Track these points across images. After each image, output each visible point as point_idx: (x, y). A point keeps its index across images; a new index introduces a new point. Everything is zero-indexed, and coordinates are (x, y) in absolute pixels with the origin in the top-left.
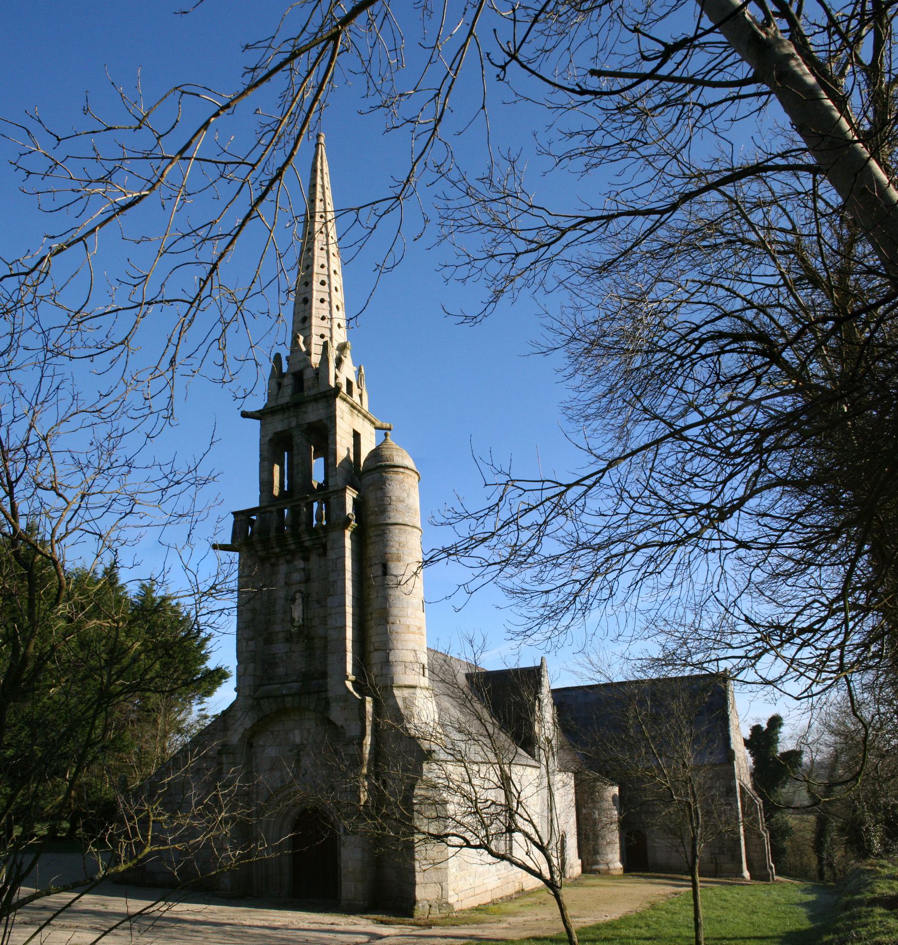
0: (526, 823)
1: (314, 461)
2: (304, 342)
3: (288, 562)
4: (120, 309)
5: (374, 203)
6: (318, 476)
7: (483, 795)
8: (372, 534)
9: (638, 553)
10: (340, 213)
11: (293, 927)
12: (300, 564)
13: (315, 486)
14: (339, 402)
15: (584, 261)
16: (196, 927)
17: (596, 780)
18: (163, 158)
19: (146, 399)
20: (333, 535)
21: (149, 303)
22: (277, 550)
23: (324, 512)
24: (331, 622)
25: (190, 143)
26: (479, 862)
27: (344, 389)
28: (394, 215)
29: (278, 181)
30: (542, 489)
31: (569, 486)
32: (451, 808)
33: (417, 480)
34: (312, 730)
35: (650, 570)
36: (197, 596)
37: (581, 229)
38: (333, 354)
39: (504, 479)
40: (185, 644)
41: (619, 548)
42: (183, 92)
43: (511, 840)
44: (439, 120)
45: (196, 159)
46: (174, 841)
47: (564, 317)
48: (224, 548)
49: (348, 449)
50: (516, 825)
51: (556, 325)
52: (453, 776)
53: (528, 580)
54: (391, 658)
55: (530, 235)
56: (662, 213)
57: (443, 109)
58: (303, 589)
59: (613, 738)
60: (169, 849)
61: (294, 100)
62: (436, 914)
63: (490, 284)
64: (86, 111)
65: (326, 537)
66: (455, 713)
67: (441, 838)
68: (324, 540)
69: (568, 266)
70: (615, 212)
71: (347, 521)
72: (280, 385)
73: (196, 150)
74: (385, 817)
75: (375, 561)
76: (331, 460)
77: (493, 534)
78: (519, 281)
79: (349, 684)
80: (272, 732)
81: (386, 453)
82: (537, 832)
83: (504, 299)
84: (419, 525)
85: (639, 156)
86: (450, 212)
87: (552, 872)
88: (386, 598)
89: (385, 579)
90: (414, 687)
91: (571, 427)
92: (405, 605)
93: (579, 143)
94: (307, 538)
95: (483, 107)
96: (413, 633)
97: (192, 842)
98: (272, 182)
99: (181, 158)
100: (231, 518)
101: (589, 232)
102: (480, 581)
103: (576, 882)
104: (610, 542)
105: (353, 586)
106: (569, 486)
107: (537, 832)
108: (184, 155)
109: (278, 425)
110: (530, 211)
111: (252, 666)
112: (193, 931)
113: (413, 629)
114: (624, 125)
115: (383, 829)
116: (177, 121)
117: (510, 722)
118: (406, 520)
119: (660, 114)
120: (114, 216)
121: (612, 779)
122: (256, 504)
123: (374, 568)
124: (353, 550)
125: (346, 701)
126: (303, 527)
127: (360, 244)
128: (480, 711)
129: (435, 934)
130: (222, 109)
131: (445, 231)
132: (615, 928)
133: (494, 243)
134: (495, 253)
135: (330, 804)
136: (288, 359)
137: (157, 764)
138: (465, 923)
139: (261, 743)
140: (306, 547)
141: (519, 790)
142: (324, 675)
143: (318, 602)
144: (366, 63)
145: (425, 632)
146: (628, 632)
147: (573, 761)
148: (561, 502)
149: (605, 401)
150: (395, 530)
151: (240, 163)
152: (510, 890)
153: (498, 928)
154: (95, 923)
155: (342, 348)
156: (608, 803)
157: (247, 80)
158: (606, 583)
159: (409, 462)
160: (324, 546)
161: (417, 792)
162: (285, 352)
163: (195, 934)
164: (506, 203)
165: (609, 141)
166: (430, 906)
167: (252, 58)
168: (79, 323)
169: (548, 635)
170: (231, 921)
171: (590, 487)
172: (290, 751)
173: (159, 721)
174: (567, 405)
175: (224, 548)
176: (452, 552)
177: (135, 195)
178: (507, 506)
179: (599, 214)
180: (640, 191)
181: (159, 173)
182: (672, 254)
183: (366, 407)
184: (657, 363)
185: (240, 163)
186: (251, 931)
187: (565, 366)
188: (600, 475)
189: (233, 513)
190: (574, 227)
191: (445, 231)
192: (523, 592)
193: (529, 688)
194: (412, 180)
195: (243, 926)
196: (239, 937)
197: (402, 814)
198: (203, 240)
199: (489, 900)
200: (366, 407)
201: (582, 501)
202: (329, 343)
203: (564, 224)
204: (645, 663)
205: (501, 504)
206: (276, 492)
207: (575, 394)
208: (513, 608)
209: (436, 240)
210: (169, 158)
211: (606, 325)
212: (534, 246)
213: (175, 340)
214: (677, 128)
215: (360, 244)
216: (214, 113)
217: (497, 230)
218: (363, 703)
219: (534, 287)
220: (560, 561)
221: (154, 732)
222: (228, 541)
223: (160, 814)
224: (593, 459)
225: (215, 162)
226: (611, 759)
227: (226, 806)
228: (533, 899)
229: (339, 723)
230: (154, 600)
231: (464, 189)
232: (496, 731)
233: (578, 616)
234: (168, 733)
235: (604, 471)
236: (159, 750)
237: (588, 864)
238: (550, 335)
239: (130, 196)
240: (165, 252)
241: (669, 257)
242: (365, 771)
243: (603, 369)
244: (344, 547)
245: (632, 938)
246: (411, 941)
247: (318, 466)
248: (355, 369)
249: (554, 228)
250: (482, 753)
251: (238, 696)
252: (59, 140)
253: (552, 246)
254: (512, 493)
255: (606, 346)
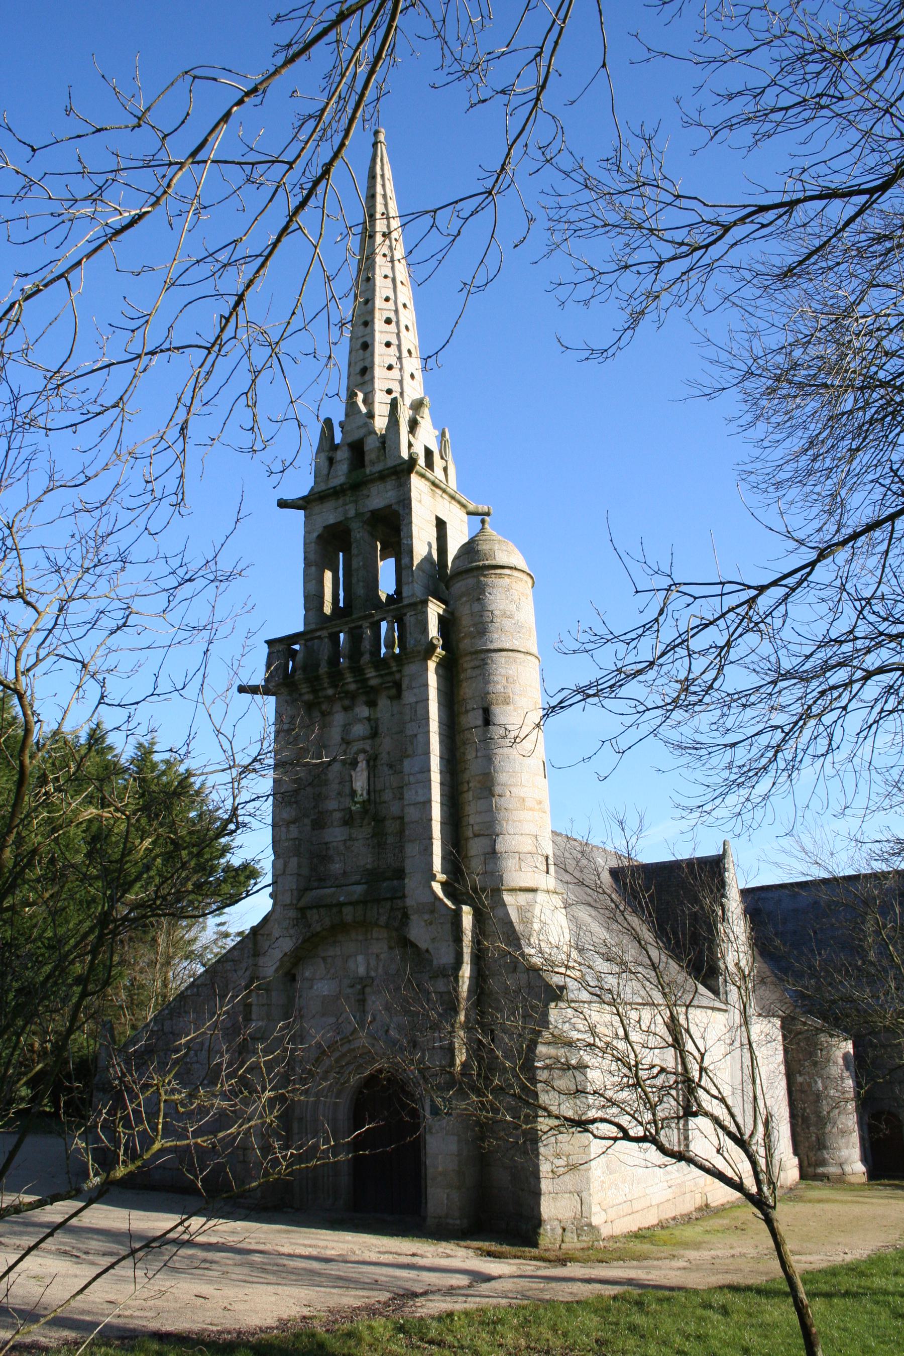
0: (715, 1102)
1: (381, 564)
2: (365, 401)
3: (346, 709)
4: (113, 364)
5: (456, 202)
6: (386, 585)
7: (647, 1058)
8: (465, 665)
9: (869, 682)
10: (408, 218)
11: (353, 1258)
12: (363, 711)
13: (383, 598)
14: (414, 478)
15: (759, 267)
16: (210, 1255)
17: (819, 1031)
18: (170, 164)
19: (147, 482)
20: (410, 669)
21: (153, 353)
22: (330, 692)
23: (396, 634)
24: (410, 795)
25: (205, 141)
26: (643, 1163)
27: (421, 461)
28: (486, 215)
29: (324, 182)
30: (722, 595)
31: (762, 589)
32: (593, 1075)
33: (530, 585)
34: (382, 956)
35: (889, 707)
36: (235, 772)
37: (752, 222)
38: (405, 415)
39: (666, 582)
40: (223, 840)
41: (840, 676)
42: (195, 77)
43: (686, 1130)
44: (543, 87)
45: (213, 162)
46: (196, 1134)
47: (735, 345)
48: (253, 690)
49: (430, 544)
50: (699, 1105)
51: (724, 357)
52: (600, 1029)
53: (704, 728)
54: (499, 847)
55: (679, 236)
56: (871, 191)
57: (548, 72)
58: (368, 748)
59: (844, 965)
60: (189, 1145)
61: (343, 75)
62: (572, 1243)
63: (624, 304)
64: (68, 111)
65: (400, 671)
66: (599, 932)
67: (582, 1124)
68: (397, 676)
69: (737, 275)
70: (801, 195)
71: (432, 647)
72: (331, 461)
73: (213, 151)
74: (499, 1091)
75: (471, 705)
76: (405, 561)
77: (652, 663)
78: (666, 299)
79: (437, 887)
80: (324, 959)
81: (484, 547)
82: (732, 1116)
83: (646, 323)
84: (534, 650)
85: (833, 114)
86: (563, 212)
87: (758, 1182)
88: (489, 759)
89: (487, 731)
90: (533, 890)
91: (755, 499)
92: (518, 769)
93: (740, 106)
94: (374, 674)
95: (604, 65)
96: (531, 809)
97: (221, 1135)
98: (316, 183)
99: (193, 163)
100: (265, 649)
101: (763, 226)
102: (633, 735)
103: (792, 1194)
104: (826, 668)
105: (441, 742)
106: (762, 589)
107: (732, 1116)
108: (198, 158)
109: (329, 515)
110: (677, 203)
111: (294, 862)
112: (205, 1261)
113: (529, 803)
114: (808, 77)
115: (496, 1111)
116: (188, 114)
117: (684, 945)
118: (516, 644)
119: (860, 56)
120: (106, 242)
121: (845, 1030)
122: (300, 628)
123: (471, 715)
124: (439, 690)
125: (432, 912)
126: (366, 658)
127: (439, 256)
128: (638, 929)
129: (572, 1275)
130: (248, 94)
131: (557, 238)
132: (862, 1274)
133: (628, 250)
134: (629, 263)
135: (413, 1071)
136: (341, 424)
137: (156, 1004)
138: (620, 1259)
139: (307, 974)
140: (372, 687)
141: (703, 1051)
142: (400, 874)
143: (391, 766)
144: (439, 25)
145: (547, 805)
146: (860, 801)
147: (781, 1001)
148: (751, 613)
149: (804, 461)
150: (500, 658)
151: (273, 162)
152: (688, 1205)
153: (671, 1269)
154: (64, 1244)
155: (417, 406)
156: (837, 1068)
157: (280, 59)
158: (821, 728)
159: (515, 558)
160: (398, 685)
161: (542, 1049)
162: (338, 414)
163: (207, 1265)
164: (642, 195)
165: (787, 100)
166: (564, 1230)
167: (286, 32)
168: (58, 386)
169: (737, 810)
170: (261, 1247)
171: (793, 590)
172: (352, 986)
173: (160, 940)
174: (748, 468)
175: (253, 690)
176: (591, 692)
177: (133, 213)
178: (671, 622)
179: (777, 199)
180: (835, 164)
181: (164, 183)
182: (890, 250)
183: (453, 484)
184: (877, 404)
185: (273, 162)
186: (292, 1263)
187: (741, 413)
188: (808, 570)
189: (266, 642)
190: (742, 220)
191: (557, 238)
192: (697, 746)
193: (712, 891)
194: (508, 168)
195: (281, 1254)
196: (274, 1273)
197: (524, 1088)
198: (225, 266)
199: (655, 1222)
200: (453, 484)
201: (782, 608)
202: (400, 400)
203: (727, 217)
204: (887, 847)
205: (661, 619)
206: (328, 609)
207: (757, 452)
208: (683, 771)
209: (546, 250)
210: (177, 163)
211: (797, 353)
212: (684, 249)
213: (186, 400)
214: (887, 75)
215: (439, 256)
216: (236, 100)
217: (631, 232)
218: (457, 916)
219: (688, 305)
220: (753, 699)
221: (153, 957)
222: (259, 679)
223: (173, 1091)
224: (793, 545)
225: (240, 163)
226: (841, 999)
227: (270, 1082)
228: (725, 1222)
229: (423, 945)
230: (154, 766)
231: (582, 181)
232: (664, 958)
233: (781, 780)
234: (172, 958)
235: (813, 564)
236: (159, 983)
237: (809, 1165)
238: (715, 370)
239: (127, 214)
240: (173, 284)
241: (886, 254)
242: (462, 1017)
243: (797, 413)
244: (426, 685)
245: (893, 1294)
246: (534, 1286)
247: (386, 570)
248: (437, 433)
249: (713, 224)
250: (643, 993)
251: (274, 905)
252: (34, 150)
253: (710, 248)
254: (678, 602)
255: (800, 383)
